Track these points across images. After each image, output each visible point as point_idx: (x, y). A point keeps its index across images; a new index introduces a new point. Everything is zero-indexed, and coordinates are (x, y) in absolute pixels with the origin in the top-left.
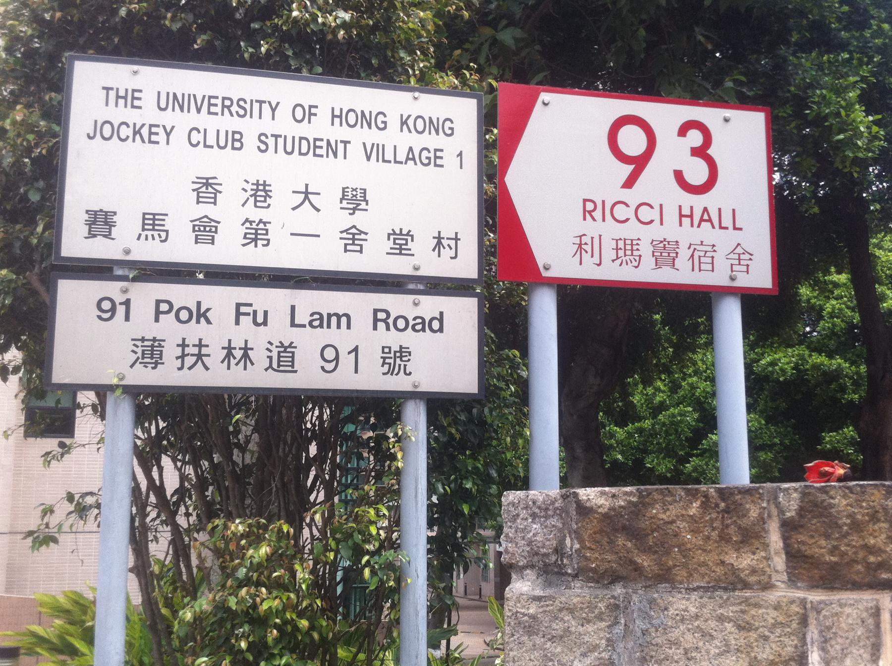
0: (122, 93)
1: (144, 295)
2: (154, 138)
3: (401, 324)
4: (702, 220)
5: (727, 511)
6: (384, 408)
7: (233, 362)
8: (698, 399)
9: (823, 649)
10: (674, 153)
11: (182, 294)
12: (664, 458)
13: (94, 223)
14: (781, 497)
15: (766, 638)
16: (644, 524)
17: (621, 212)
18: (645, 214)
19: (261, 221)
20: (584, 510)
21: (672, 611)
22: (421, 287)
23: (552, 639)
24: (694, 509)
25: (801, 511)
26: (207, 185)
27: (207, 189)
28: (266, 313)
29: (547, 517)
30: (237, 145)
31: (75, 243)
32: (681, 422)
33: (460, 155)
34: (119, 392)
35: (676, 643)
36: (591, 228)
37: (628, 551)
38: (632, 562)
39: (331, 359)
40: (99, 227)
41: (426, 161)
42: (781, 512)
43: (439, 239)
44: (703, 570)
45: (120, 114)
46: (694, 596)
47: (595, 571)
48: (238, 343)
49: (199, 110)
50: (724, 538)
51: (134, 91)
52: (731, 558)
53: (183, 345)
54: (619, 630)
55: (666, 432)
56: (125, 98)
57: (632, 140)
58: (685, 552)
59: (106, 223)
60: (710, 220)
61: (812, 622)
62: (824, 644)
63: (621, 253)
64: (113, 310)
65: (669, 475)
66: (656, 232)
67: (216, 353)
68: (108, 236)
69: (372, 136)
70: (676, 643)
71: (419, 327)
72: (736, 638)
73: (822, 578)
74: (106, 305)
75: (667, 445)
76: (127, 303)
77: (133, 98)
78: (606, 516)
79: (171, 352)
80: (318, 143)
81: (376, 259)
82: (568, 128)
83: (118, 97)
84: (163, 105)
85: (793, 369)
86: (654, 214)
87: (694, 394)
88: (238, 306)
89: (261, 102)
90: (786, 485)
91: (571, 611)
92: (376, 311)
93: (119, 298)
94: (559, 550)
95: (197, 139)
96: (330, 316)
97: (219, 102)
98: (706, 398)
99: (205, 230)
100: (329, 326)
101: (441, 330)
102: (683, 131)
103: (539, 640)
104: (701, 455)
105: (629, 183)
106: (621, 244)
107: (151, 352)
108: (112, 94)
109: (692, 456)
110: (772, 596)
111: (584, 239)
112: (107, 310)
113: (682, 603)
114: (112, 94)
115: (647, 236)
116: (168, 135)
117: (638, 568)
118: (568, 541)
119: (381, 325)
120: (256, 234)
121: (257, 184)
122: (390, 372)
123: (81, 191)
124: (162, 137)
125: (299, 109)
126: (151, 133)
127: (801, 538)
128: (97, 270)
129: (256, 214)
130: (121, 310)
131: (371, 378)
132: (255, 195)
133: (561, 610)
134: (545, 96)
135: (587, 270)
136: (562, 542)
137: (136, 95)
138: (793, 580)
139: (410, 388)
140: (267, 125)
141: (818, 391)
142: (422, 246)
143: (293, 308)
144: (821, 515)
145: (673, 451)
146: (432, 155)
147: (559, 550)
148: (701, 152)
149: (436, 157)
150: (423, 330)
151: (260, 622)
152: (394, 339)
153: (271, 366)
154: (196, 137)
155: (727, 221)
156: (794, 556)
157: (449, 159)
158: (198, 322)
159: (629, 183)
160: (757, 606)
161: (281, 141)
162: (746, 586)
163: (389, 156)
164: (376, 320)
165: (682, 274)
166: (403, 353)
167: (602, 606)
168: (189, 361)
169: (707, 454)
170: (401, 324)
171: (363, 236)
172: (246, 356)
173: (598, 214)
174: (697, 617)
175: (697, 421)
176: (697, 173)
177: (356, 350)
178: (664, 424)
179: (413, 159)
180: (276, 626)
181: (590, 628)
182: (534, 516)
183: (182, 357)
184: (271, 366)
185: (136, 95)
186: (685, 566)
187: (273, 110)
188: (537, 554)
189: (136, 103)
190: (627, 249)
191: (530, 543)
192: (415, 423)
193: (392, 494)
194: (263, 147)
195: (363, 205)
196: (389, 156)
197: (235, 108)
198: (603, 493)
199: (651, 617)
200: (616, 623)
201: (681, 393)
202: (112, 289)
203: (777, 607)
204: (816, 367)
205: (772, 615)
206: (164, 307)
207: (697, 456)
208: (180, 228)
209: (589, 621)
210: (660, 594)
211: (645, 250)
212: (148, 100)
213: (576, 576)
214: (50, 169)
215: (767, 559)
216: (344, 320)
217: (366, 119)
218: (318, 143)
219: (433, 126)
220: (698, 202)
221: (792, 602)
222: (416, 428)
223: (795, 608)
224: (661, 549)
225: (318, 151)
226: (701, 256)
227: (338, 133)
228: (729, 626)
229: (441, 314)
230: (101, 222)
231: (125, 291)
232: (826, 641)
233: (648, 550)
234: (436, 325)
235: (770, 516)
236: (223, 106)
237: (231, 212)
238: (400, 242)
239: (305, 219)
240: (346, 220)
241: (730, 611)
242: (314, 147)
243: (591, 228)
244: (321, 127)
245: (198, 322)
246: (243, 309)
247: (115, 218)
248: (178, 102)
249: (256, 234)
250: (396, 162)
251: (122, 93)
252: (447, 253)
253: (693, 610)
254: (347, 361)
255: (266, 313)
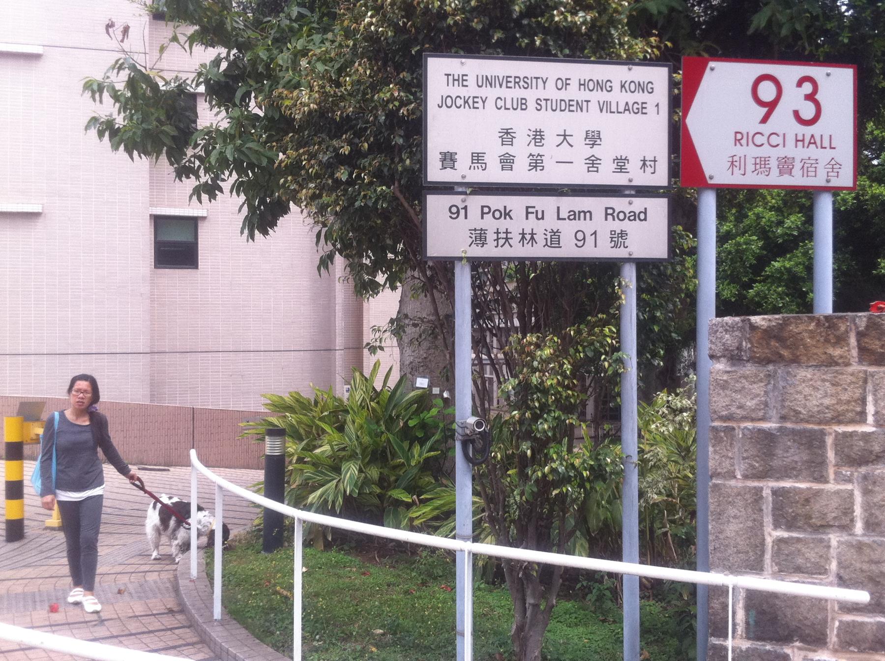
0: (456, 77)
1: (476, 202)
2: (476, 105)
3: (621, 216)
4: (810, 143)
5: (829, 327)
6: (608, 269)
7: (526, 242)
8: (763, 228)
9: (875, 395)
10: (794, 98)
11: (496, 202)
12: (729, 284)
13: (445, 160)
14: (857, 320)
15: (846, 390)
16: (786, 334)
17: (759, 140)
18: (774, 140)
19: (539, 155)
20: (753, 327)
21: (798, 377)
22: (633, 192)
23: (736, 392)
24: (812, 326)
25: (867, 327)
26: (507, 133)
27: (507, 135)
28: (543, 212)
29: (733, 331)
30: (524, 107)
31: (435, 173)
32: (746, 250)
33: (657, 105)
34: (464, 262)
35: (800, 392)
36: (740, 151)
37: (777, 348)
38: (779, 353)
39: (581, 239)
40: (448, 163)
41: (636, 111)
42: (857, 328)
43: (644, 161)
44: (815, 357)
45: (456, 91)
46: (810, 370)
47: (758, 358)
48: (528, 231)
49: (501, 86)
50: (827, 341)
51: (463, 75)
52: (830, 351)
53: (498, 233)
54: (770, 387)
55: (732, 259)
56: (458, 80)
57: (767, 91)
58: (806, 347)
59: (451, 160)
60: (815, 143)
61: (870, 381)
62: (875, 392)
63: (758, 166)
64: (458, 212)
65: (733, 300)
66: (781, 152)
67: (516, 238)
68: (453, 168)
69: (603, 96)
70: (800, 392)
71: (632, 218)
72: (830, 389)
73: (876, 360)
74: (454, 210)
75: (732, 272)
76: (465, 208)
77: (463, 80)
78: (765, 331)
79: (491, 237)
80: (571, 103)
81: (606, 176)
82: (727, 82)
83: (454, 80)
84: (480, 84)
85: (854, 199)
86: (779, 140)
87: (759, 224)
88: (527, 208)
89: (537, 78)
90: (860, 314)
91: (746, 377)
92: (607, 209)
93: (461, 206)
94: (739, 348)
95: (501, 105)
96: (580, 212)
97: (512, 80)
98: (770, 227)
99: (507, 162)
100: (579, 219)
101: (645, 219)
102: (800, 84)
103: (728, 392)
104: (764, 281)
105: (764, 120)
106: (758, 161)
107: (480, 237)
108: (451, 78)
109: (755, 282)
110: (850, 369)
111: (735, 159)
112: (455, 213)
113: (804, 373)
114: (451, 78)
115: (774, 154)
116: (484, 102)
117: (781, 357)
118: (744, 343)
119: (610, 217)
120: (536, 163)
121: (536, 131)
122: (616, 246)
123: (438, 139)
124: (480, 105)
125: (560, 81)
126: (474, 102)
127: (866, 340)
128: (446, 188)
129: (535, 150)
130: (462, 212)
131: (604, 250)
132: (534, 139)
133: (740, 377)
134: (712, 64)
135: (737, 179)
136: (741, 344)
137: (465, 78)
138: (861, 361)
139: (627, 256)
140: (541, 94)
141: (876, 220)
142: (634, 166)
143: (558, 208)
144: (877, 329)
145: (737, 277)
146: (640, 106)
147: (739, 348)
148: (811, 97)
149: (643, 108)
150: (635, 219)
151: (545, 391)
152: (617, 226)
153: (547, 244)
154: (500, 103)
155: (826, 143)
156: (862, 350)
157: (651, 109)
158: (505, 218)
159: (764, 120)
160: (842, 374)
161: (549, 102)
162: (837, 364)
163: (614, 109)
164: (607, 214)
165: (797, 179)
166: (623, 234)
167: (762, 375)
168: (501, 242)
169: (769, 280)
170: (621, 216)
171: (598, 162)
172: (532, 238)
173: (744, 141)
174: (811, 380)
175: (761, 248)
176: (808, 111)
177: (595, 233)
178: (730, 253)
179: (628, 110)
180: (552, 395)
181: (755, 386)
182: (726, 331)
183: (497, 239)
184: (547, 244)
185: (465, 78)
186: (806, 355)
187: (544, 83)
188: (727, 350)
189: (465, 83)
190: (762, 164)
191: (724, 344)
192: (629, 276)
193: (616, 320)
194: (539, 107)
195: (598, 142)
196: (614, 109)
197: (522, 83)
198: (764, 319)
199: (787, 380)
200: (769, 383)
201: (747, 222)
202: (456, 200)
203: (852, 374)
204: (874, 197)
205: (849, 378)
206: (486, 210)
207: (760, 282)
208: (492, 161)
209: (755, 383)
210: (793, 369)
211: (773, 164)
212: (471, 81)
213: (748, 361)
214: (416, 127)
215: (848, 351)
216: (588, 214)
217: (600, 86)
218: (571, 103)
219: (641, 87)
220: (808, 130)
221: (860, 372)
222: (631, 281)
223: (861, 375)
224: (793, 347)
225: (571, 108)
226: (809, 166)
227: (584, 95)
228: (827, 384)
229: (646, 209)
230: (448, 159)
231: (464, 201)
232: (876, 391)
233: (787, 347)
234: (642, 216)
235: (851, 330)
236: (515, 82)
237: (521, 150)
238: (621, 164)
239: (564, 152)
240: (588, 152)
241: (828, 377)
242: (569, 106)
243: (740, 151)
244: (573, 93)
245: (505, 218)
246: (530, 210)
247: (456, 157)
248: (489, 81)
249: (536, 163)
250: (618, 112)
251: (456, 77)
252: (649, 170)
253: (809, 376)
254: (590, 240)
255: (543, 212)
